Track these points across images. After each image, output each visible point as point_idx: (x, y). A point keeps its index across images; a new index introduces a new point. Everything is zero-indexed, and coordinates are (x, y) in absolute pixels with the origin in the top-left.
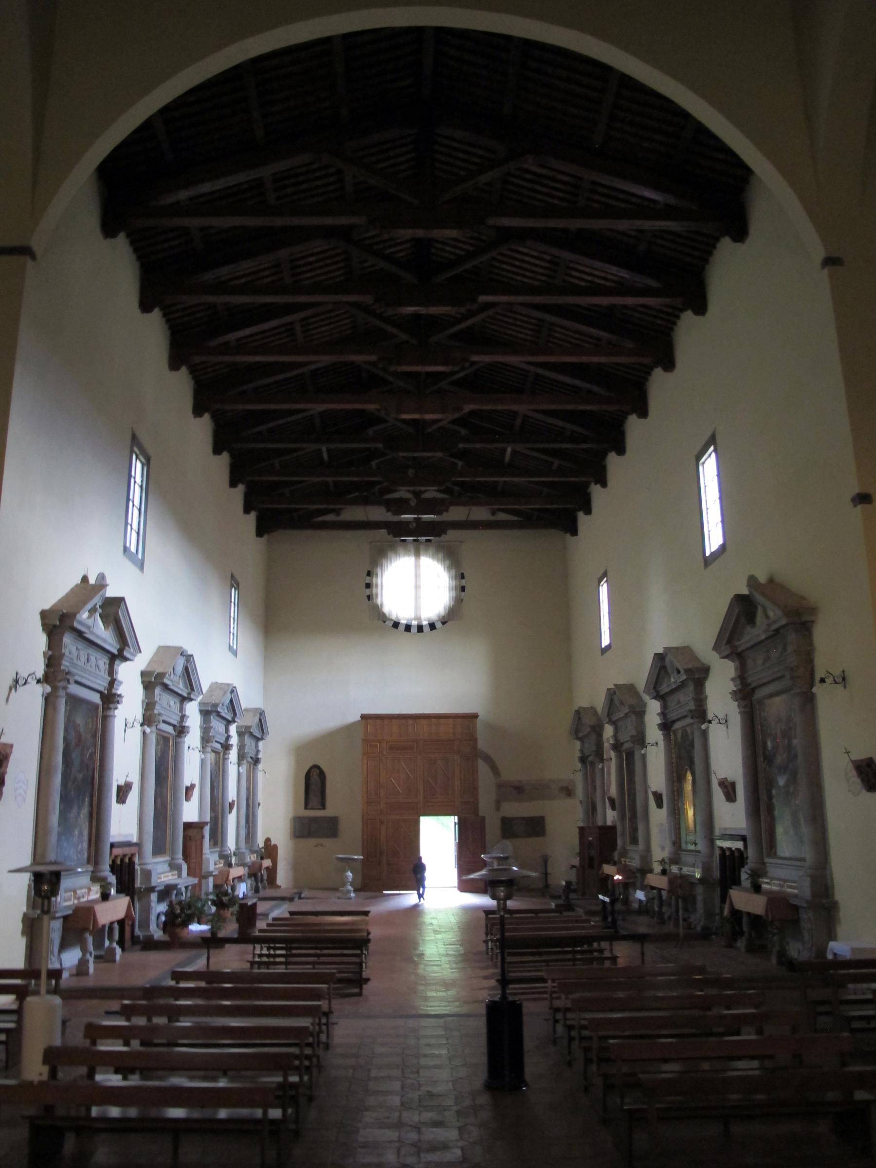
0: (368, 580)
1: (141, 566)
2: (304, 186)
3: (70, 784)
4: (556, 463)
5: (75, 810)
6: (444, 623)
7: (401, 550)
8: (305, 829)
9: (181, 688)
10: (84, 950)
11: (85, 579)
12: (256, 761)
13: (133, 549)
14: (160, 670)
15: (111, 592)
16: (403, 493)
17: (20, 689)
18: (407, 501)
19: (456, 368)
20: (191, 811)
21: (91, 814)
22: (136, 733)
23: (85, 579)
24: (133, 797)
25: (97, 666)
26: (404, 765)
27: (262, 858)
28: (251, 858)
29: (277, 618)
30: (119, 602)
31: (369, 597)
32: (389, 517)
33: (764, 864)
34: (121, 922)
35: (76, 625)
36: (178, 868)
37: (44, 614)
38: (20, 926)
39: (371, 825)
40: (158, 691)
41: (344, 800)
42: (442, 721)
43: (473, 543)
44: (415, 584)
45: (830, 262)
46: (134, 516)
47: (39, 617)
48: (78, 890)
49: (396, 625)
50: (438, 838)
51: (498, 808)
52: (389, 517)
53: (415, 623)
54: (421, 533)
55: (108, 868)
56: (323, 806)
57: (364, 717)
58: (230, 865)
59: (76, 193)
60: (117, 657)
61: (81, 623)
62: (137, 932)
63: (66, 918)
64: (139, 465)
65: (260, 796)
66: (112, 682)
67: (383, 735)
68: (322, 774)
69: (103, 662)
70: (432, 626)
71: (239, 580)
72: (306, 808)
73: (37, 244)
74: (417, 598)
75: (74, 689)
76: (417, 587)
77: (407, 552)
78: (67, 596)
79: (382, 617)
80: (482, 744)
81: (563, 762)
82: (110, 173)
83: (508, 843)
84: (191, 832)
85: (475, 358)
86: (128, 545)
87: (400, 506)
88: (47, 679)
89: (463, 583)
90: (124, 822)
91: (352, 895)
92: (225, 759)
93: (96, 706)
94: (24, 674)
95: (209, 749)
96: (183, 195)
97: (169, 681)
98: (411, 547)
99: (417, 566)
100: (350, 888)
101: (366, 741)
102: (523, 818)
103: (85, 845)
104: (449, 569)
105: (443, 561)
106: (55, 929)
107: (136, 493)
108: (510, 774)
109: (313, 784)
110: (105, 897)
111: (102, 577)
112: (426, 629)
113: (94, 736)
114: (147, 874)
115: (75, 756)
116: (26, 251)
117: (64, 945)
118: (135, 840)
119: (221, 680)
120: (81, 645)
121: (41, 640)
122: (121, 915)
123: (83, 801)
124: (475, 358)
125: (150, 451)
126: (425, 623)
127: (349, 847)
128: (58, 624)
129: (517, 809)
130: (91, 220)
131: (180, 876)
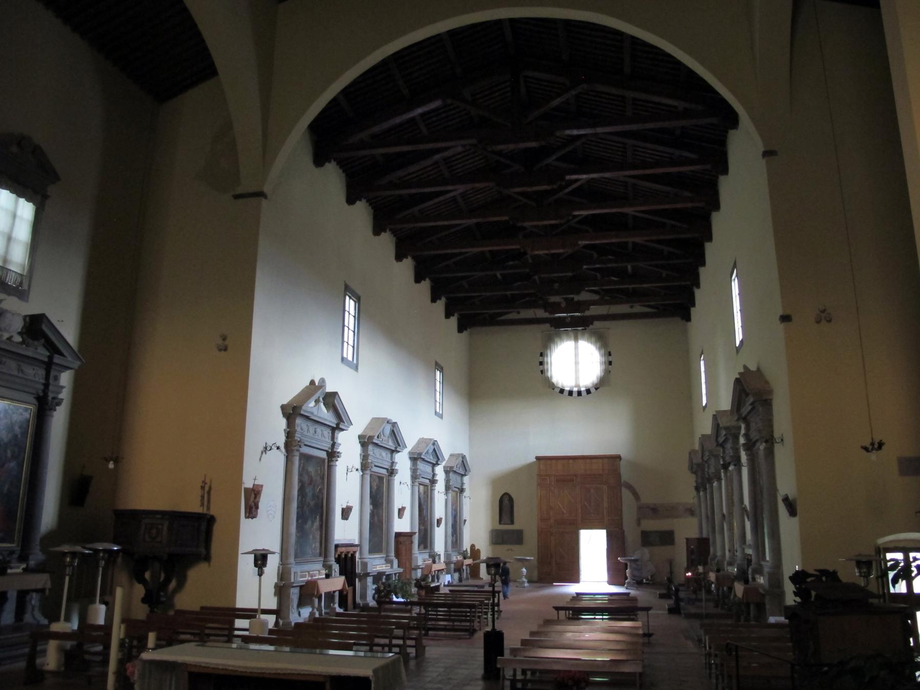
0: (541, 359)
1: (356, 368)
2: (443, 115)
3: (305, 507)
4: (664, 273)
5: (309, 523)
6: (596, 389)
7: (564, 337)
8: (498, 538)
9: (391, 445)
10: (313, 607)
11: (312, 382)
12: (462, 490)
13: (350, 358)
14: (371, 434)
15: (329, 389)
16: (554, 299)
17: (268, 453)
18: (559, 304)
19: (562, 222)
20: (402, 525)
21: (321, 526)
22: (356, 476)
23: (312, 382)
24: (355, 515)
25: (322, 434)
26: (569, 492)
27: (465, 558)
28: (456, 558)
29: (477, 390)
30: (334, 395)
31: (542, 372)
32: (546, 315)
33: (761, 565)
34: (341, 592)
35: (302, 412)
36: (391, 562)
37: (283, 407)
38: (273, 590)
39: (543, 534)
40: (370, 447)
41: (526, 518)
42: (594, 461)
43: (616, 329)
44: (575, 361)
45: (767, 154)
46: (349, 336)
47: (280, 410)
48: (311, 570)
49: (562, 391)
50: (593, 545)
51: (639, 524)
52: (546, 315)
53: (575, 389)
54: (579, 324)
55: (333, 559)
56: (512, 523)
57: (538, 458)
58: (434, 562)
59: (296, 141)
60: (335, 429)
61: (309, 410)
62: (358, 600)
63: (301, 587)
64: (352, 303)
65: (466, 514)
66: (333, 445)
67: (553, 472)
68: (511, 500)
69: (327, 433)
70: (588, 391)
71: (442, 365)
72: (500, 523)
73: (266, 189)
74: (577, 371)
75: (305, 450)
76: (577, 363)
77: (569, 338)
78: (299, 395)
79: (552, 386)
80: (625, 477)
81: (684, 490)
82: (315, 127)
83: (646, 551)
84: (401, 539)
85: (576, 213)
86: (345, 356)
87: (555, 308)
88: (287, 445)
89: (610, 359)
90: (346, 531)
91: (526, 584)
92: (432, 490)
93: (323, 460)
94: (270, 444)
95: (417, 484)
96: (364, 135)
97: (381, 440)
98: (572, 334)
99: (576, 348)
100: (524, 580)
101: (539, 475)
102: (657, 532)
103: (318, 545)
104: (600, 349)
105: (595, 343)
106: (294, 594)
107: (350, 321)
108: (648, 498)
109: (505, 506)
110: (328, 576)
111: (323, 381)
112: (584, 394)
113: (323, 478)
114: (365, 565)
115: (309, 491)
116: (261, 194)
117: (301, 604)
118: (357, 543)
119: (427, 436)
120: (310, 423)
121: (283, 422)
122: (339, 587)
123: (316, 518)
124: (576, 213)
125: (359, 292)
126: (583, 389)
127: (529, 552)
128: (292, 412)
129: (651, 525)
130: (307, 158)
131: (392, 567)
